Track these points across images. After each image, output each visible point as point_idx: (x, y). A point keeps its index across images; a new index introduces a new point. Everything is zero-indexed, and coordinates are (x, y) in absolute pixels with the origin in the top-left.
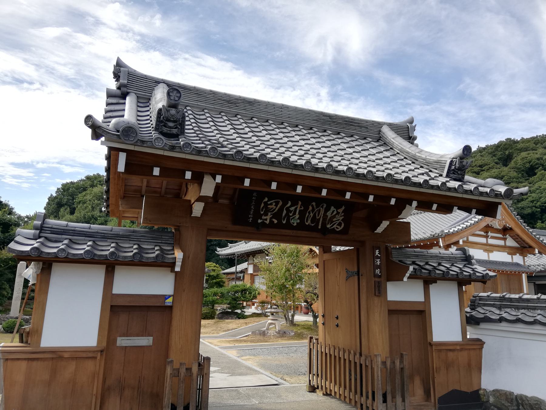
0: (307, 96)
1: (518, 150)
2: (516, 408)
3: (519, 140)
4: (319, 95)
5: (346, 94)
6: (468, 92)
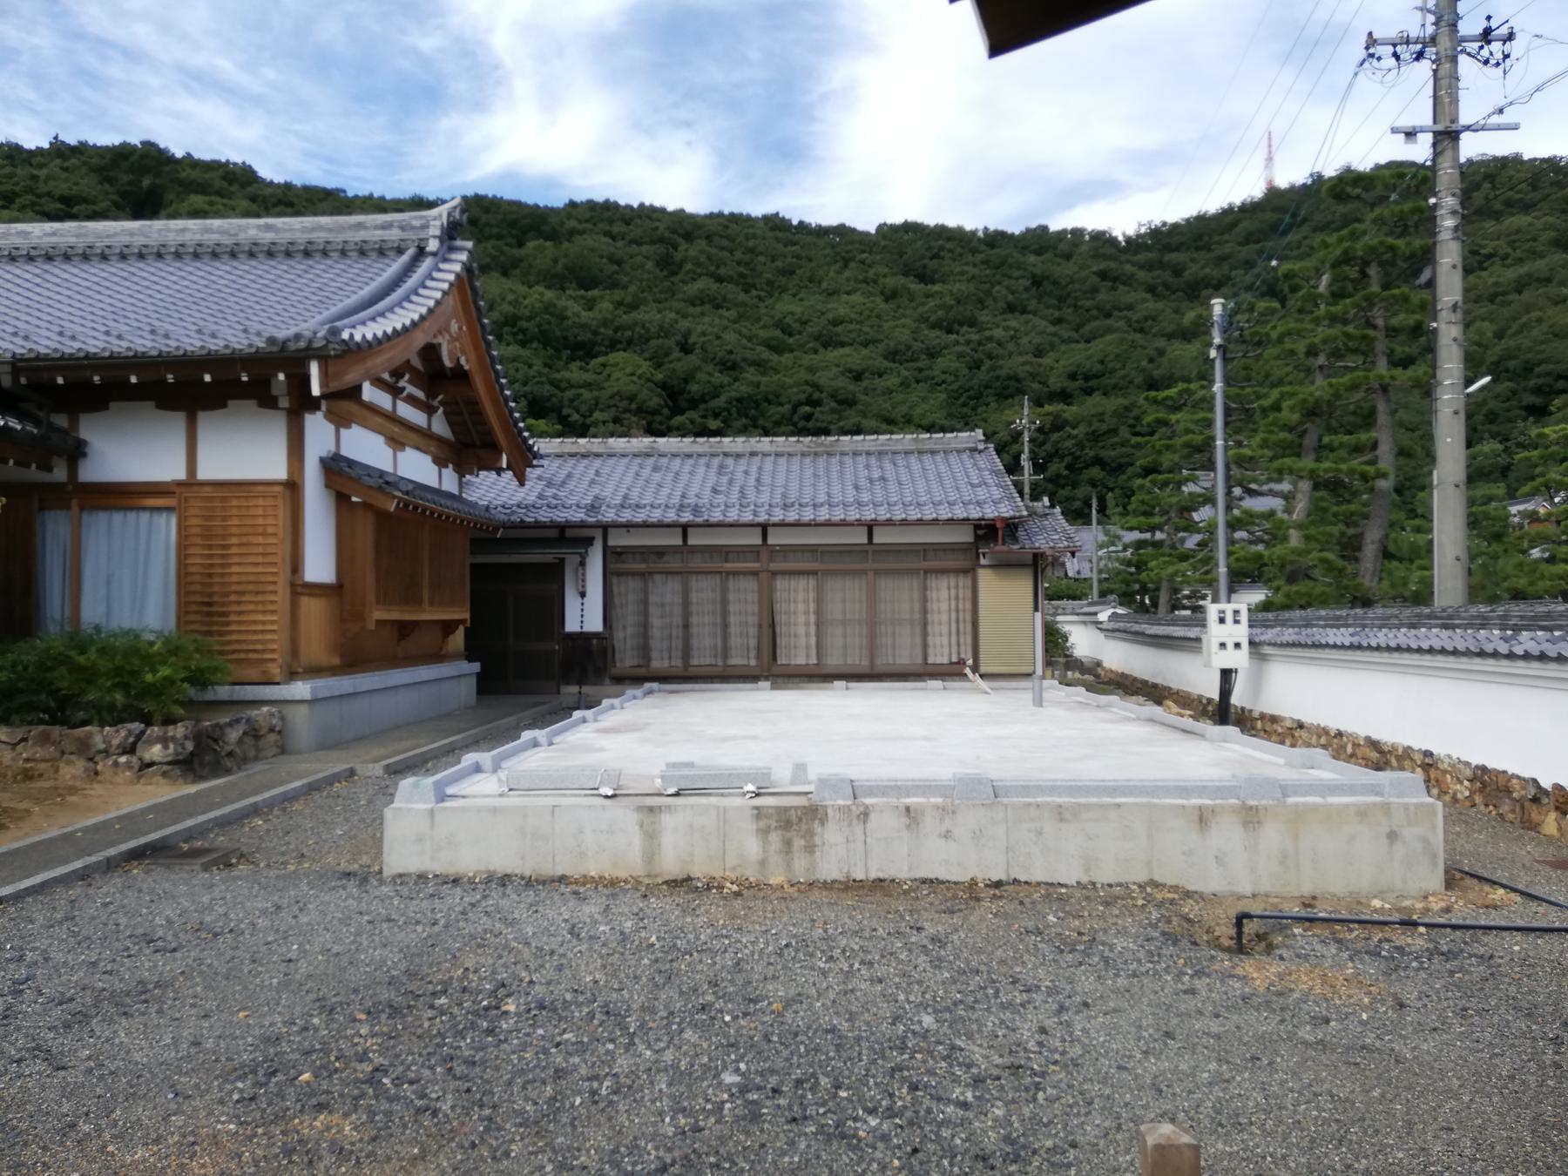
1: (181, 183)
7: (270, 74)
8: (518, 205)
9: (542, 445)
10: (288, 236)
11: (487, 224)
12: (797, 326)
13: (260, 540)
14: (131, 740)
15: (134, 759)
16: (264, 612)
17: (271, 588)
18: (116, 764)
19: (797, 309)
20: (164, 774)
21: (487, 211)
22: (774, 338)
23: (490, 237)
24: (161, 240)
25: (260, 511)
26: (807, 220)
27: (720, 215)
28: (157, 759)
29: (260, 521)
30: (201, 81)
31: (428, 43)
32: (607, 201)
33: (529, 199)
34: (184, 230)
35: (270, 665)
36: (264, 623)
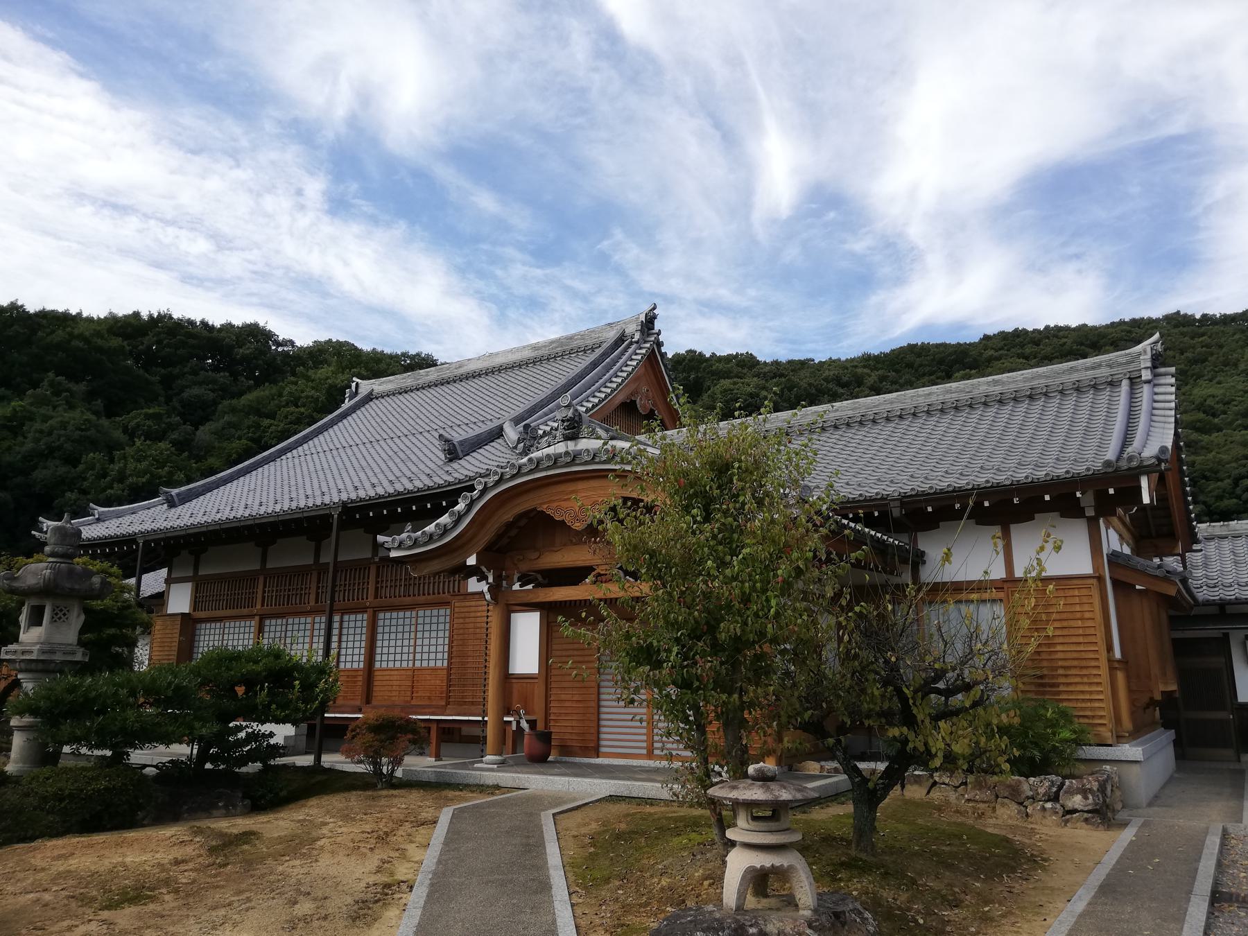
0: (271, 189)
1: (713, 373)
2: (1242, 541)
3: (708, 356)
4: (299, 192)
5: (367, 207)
6: (616, 257)
7: (752, 292)
8: (944, 345)
9: (1202, 528)
10: (1013, 387)
11: (921, 365)
12: (1220, 407)
13: (1080, 623)
14: (1054, 789)
15: (1058, 806)
16: (1091, 684)
17: (1093, 663)
18: (1044, 809)
19: (1218, 391)
20: (1086, 820)
21: (919, 355)
22: (1200, 421)
23: (924, 375)
24: (915, 403)
25: (1077, 600)
26: (1210, 312)
27: (1122, 323)
28: (1080, 808)
29: (1078, 608)
30: (711, 307)
31: (859, 246)
32: (1016, 330)
33: (952, 340)
34: (929, 394)
35: (1101, 729)
36: (1091, 693)
